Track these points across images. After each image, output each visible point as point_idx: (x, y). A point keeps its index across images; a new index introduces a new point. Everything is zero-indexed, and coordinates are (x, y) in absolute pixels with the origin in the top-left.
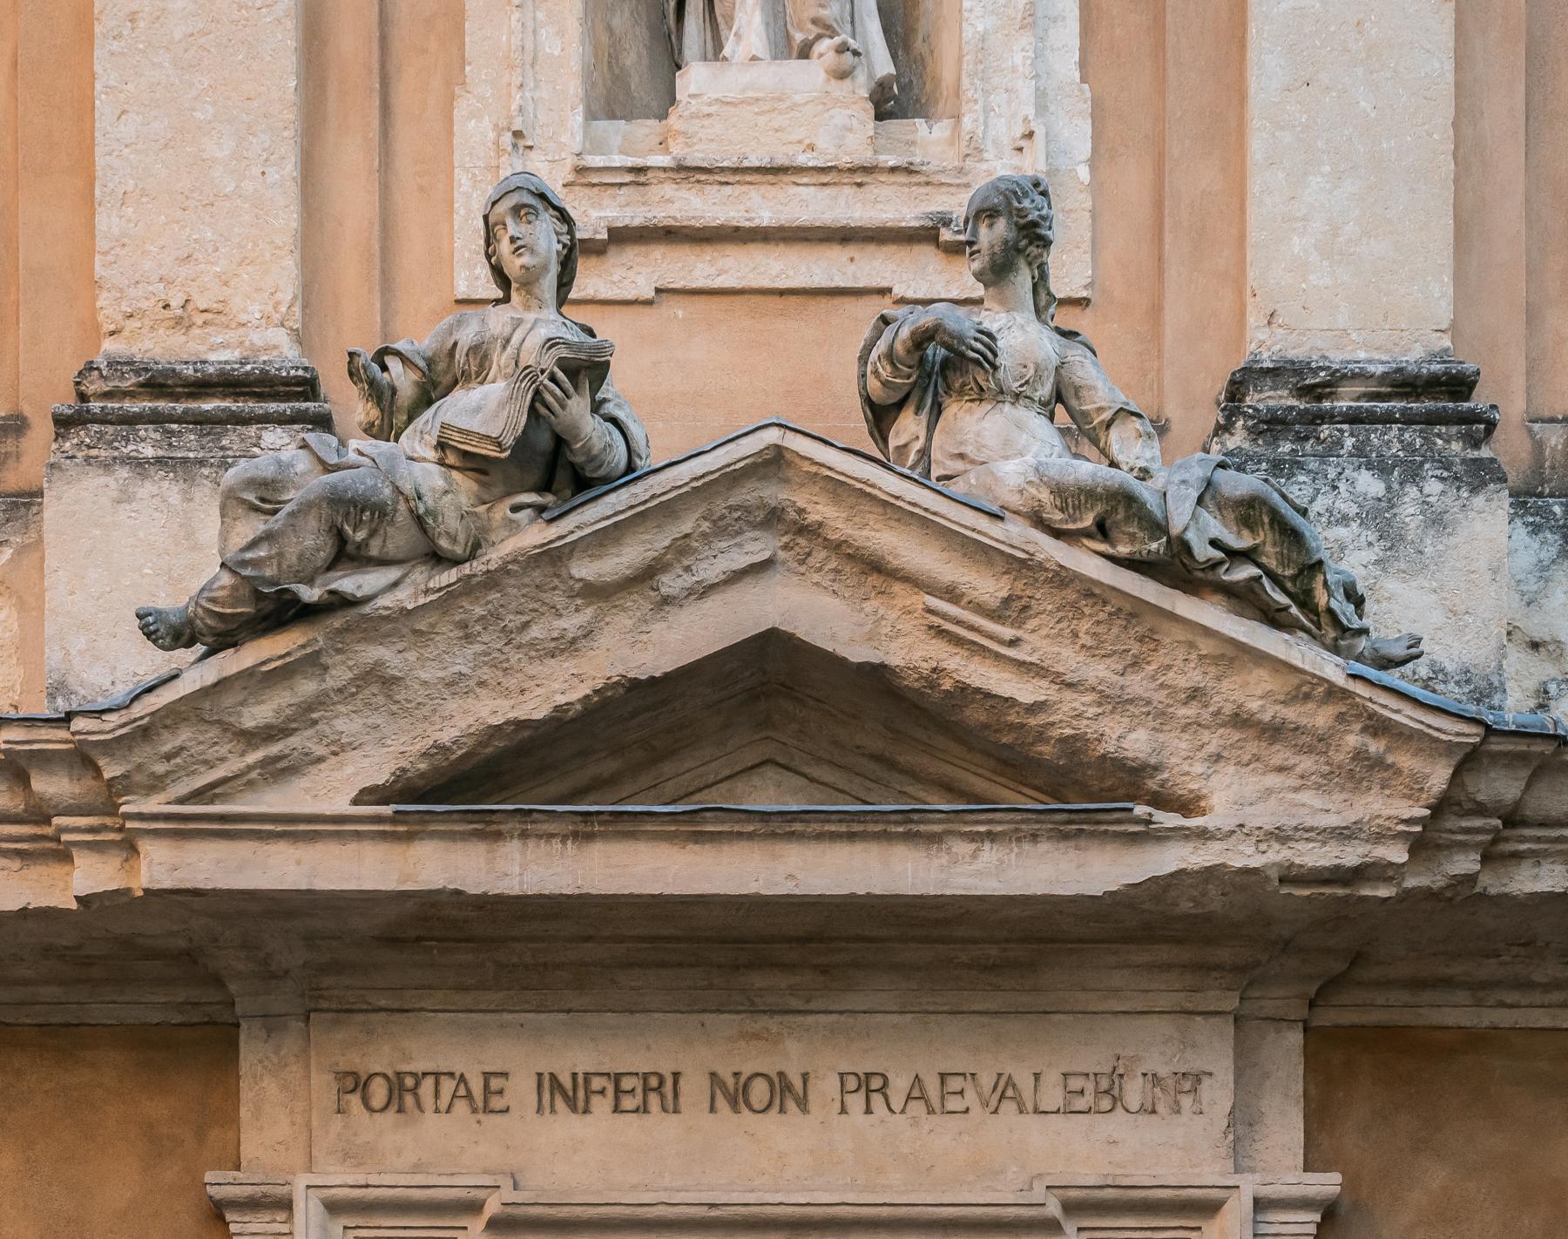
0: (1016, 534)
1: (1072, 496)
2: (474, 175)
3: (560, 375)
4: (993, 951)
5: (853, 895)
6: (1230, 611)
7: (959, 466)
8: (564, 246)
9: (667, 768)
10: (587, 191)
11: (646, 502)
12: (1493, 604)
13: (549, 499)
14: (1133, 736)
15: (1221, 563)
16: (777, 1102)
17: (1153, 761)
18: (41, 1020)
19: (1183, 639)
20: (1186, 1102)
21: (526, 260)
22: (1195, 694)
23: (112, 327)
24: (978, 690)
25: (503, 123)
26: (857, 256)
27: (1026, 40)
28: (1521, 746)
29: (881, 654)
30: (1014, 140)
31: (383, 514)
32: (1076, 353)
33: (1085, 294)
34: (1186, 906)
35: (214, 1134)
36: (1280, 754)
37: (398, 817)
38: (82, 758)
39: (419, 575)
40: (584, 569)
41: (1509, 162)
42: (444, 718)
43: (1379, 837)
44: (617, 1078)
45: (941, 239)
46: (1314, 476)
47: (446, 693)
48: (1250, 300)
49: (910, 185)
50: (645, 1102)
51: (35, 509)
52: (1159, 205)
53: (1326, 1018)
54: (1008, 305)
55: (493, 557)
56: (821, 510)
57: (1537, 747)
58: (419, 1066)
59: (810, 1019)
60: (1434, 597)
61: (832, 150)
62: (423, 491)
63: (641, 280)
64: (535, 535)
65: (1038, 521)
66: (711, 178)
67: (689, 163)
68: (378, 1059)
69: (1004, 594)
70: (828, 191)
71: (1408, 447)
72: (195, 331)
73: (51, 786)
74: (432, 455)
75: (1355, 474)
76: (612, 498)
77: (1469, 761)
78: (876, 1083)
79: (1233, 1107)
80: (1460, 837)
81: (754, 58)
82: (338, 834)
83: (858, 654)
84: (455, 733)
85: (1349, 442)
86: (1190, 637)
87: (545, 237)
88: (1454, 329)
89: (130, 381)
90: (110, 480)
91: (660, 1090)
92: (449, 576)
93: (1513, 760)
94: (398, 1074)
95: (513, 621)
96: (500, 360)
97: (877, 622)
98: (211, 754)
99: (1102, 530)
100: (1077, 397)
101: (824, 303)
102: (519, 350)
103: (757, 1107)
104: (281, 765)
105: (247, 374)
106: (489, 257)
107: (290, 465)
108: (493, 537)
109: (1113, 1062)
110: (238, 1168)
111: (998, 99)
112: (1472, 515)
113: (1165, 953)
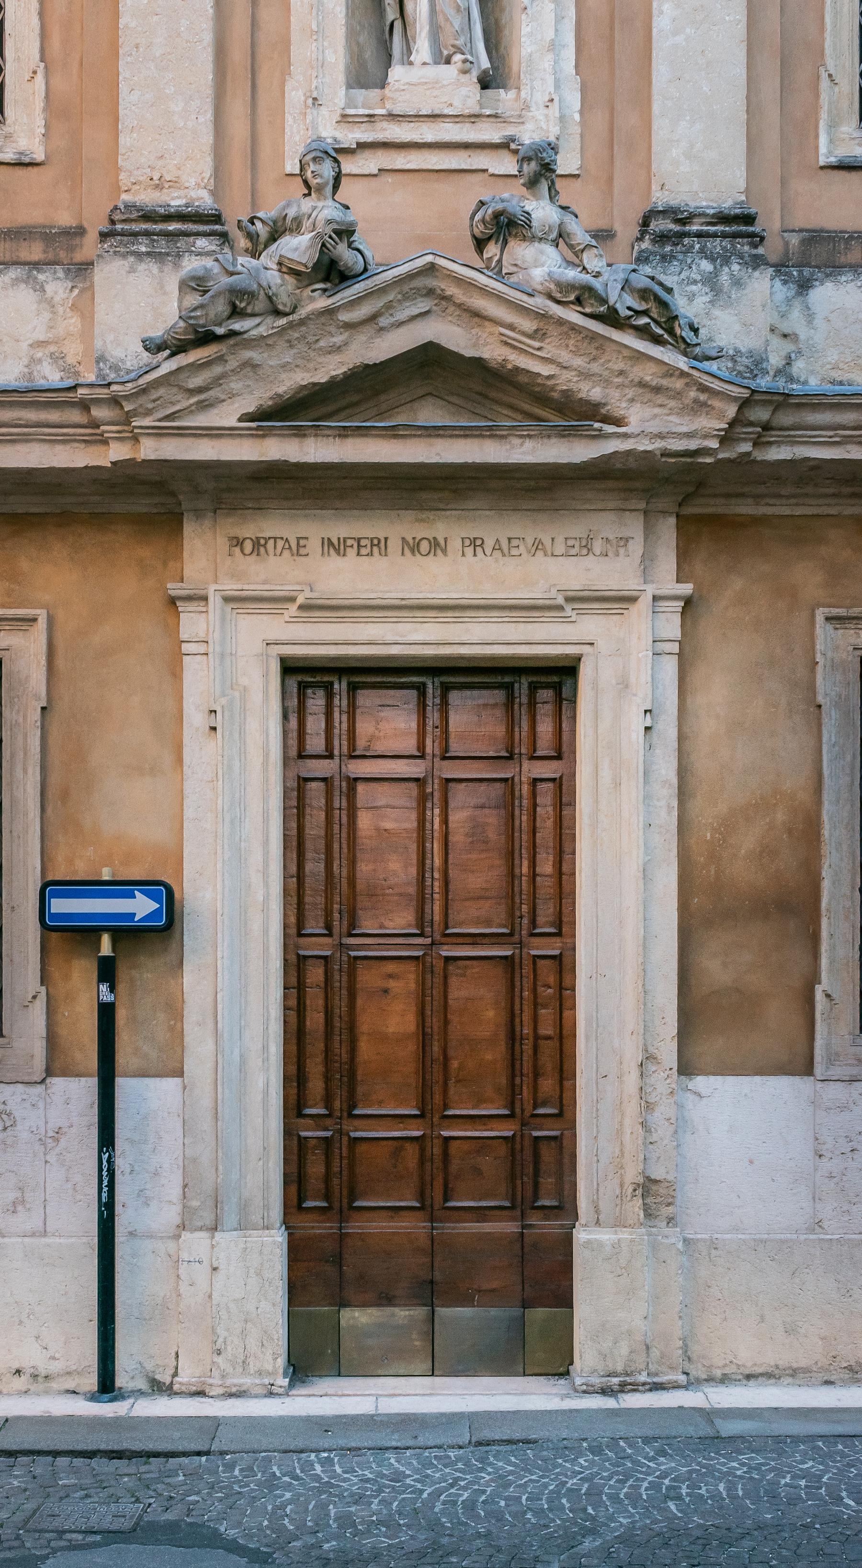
0: (539, 303)
1: (566, 287)
3: (334, 236)
4: (532, 483)
5: (466, 463)
6: (636, 337)
7: (514, 269)
9: (383, 397)
10: (347, 125)
12: (763, 319)
13: (328, 285)
14: (594, 390)
15: (632, 316)
16: (433, 551)
17: (603, 401)
18: (91, 511)
20: (622, 551)
21: (318, 180)
22: (621, 373)
23: (126, 188)
24: (523, 369)
25: (308, 94)
27: (550, 56)
28: (768, 397)
31: (253, 296)
32: (569, 219)
33: (577, 172)
34: (618, 466)
35: (171, 564)
36: (660, 399)
37: (258, 428)
38: (115, 401)
39: (269, 320)
40: (344, 317)
41: (773, 115)
42: (280, 382)
43: (705, 437)
44: (359, 540)
46: (681, 262)
47: (281, 370)
48: (653, 178)
50: (372, 551)
51: (89, 271)
52: (611, 131)
53: (688, 510)
54: (537, 197)
55: (303, 312)
56: (452, 290)
57: (776, 398)
58: (267, 534)
59: (448, 513)
60: (736, 318)
61: (460, 106)
62: (271, 285)
64: (322, 303)
65: (550, 297)
66: (404, 119)
67: (394, 113)
68: (248, 530)
69: (535, 328)
70: (458, 125)
71: (724, 248)
72: (165, 191)
73: (97, 412)
74: (275, 267)
76: (357, 286)
77: (745, 404)
78: (478, 542)
79: (643, 554)
80: (743, 436)
81: (424, 64)
82: (231, 435)
83: (468, 353)
84: (284, 388)
85: (697, 246)
86: (618, 349)
88: (747, 191)
89: (134, 215)
90: (125, 262)
91: (379, 545)
92: (283, 321)
93: (765, 403)
94: (257, 538)
95: (311, 339)
96: (307, 224)
97: (478, 339)
98: (174, 399)
99: (579, 301)
100: (568, 237)
101: (456, 176)
103: (423, 553)
104: (207, 403)
107: (211, 270)
108: (303, 303)
109: (588, 533)
110: (182, 580)
112: (753, 280)
113: (610, 484)
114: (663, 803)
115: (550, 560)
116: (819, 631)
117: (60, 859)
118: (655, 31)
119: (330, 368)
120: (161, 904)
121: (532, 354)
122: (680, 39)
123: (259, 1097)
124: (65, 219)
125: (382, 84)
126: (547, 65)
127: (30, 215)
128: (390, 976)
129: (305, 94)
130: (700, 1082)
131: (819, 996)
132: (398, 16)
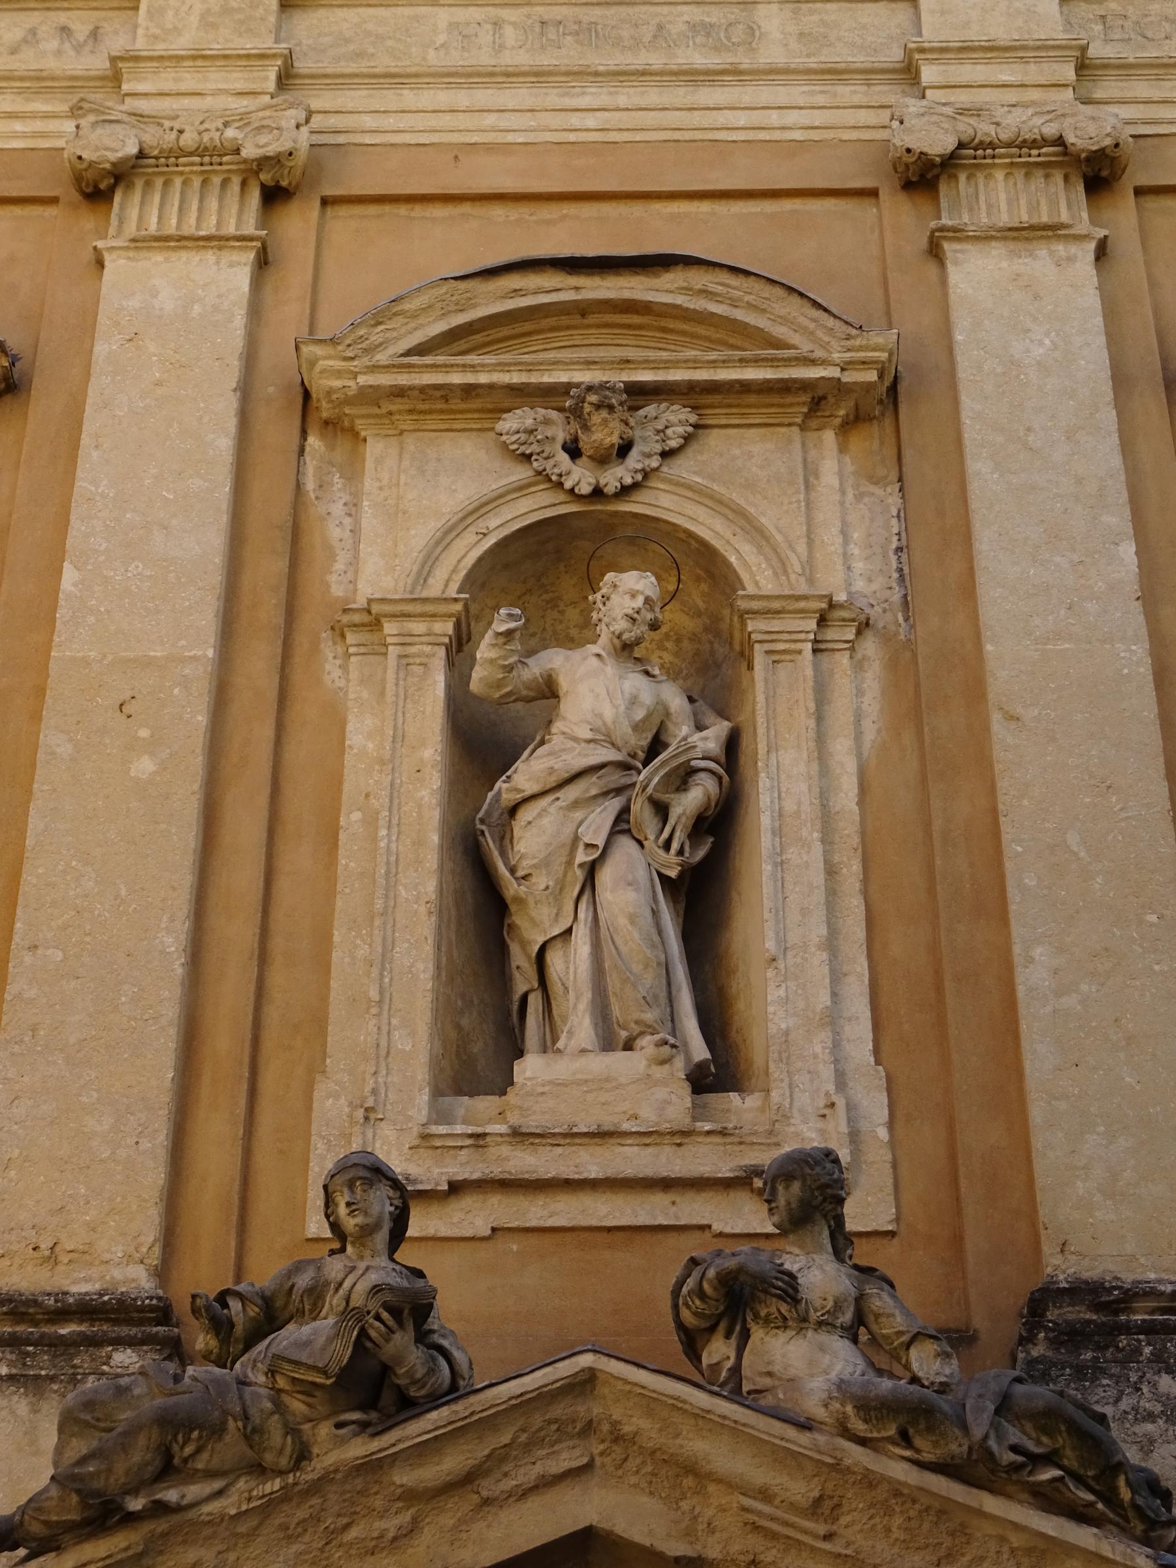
2: (329, 1141)
3: (385, 1315)
8: (397, 1207)
10: (430, 1152)
11: (466, 1417)
13: (373, 1416)
15: (1021, 1466)
19: (995, 1533)
26: (678, 1200)
29: (699, 1547)
30: (818, 1109)
40: (404, 1477)
45: (755, 1186)
46: (1117, 1379)
48: (1043, 1232)
49: (725, 1144)
61: (654, 1118)
63: (479, 1222)
70: (650, 1150)
72: (61, 1268)
75: (1156, 1378)
81: (583, 1051)
85: (1147, 1350)
87: (381, 1202)
96: (333, 1301)
102: (350, 1292)
105: (104, 1303)
106: (327, 1216)
111: (801, 1079)
121: (813, 1549)
122: (1070, 1001)
125: (503, 1083)
126: (818, 1049)
129: (350, 1104)
132: (536, 985)
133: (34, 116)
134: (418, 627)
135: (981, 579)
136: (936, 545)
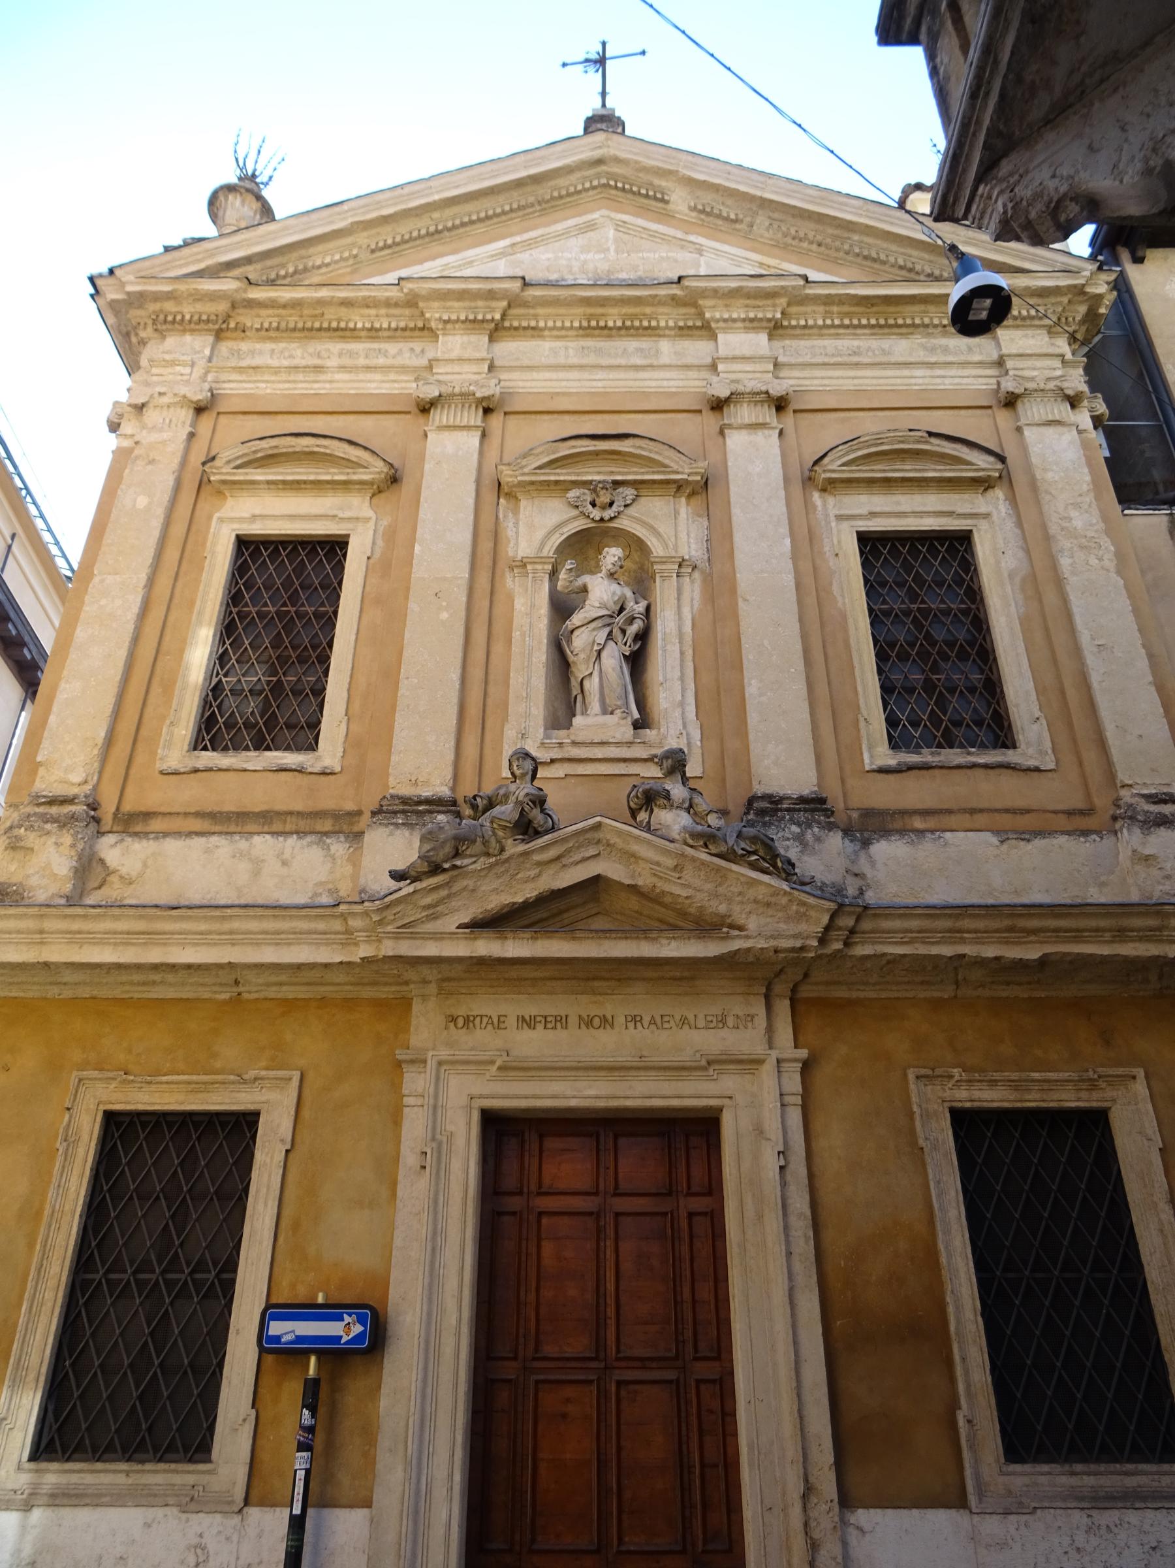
1: (695, 836)
40: (537, 857)
58: (475, 1013)
88: (819, 785)
91: (561, 1021)
114: (800, 1233)
115: (694, 1032)
116: (912, 1086)
117: (284, 1284)
118: (747, 695)
119: (525, 893)
120: (365, 1326)
122: (764, 699)
123: (442, 1531)
124: (350, 806)
127: (327, 803)
128: (568, 1400)
130: (862, 1517)
131: (961, 1422)
133: (401, 381)
134: (539, 567)
135: (736, 552)
136: (720, 539)
